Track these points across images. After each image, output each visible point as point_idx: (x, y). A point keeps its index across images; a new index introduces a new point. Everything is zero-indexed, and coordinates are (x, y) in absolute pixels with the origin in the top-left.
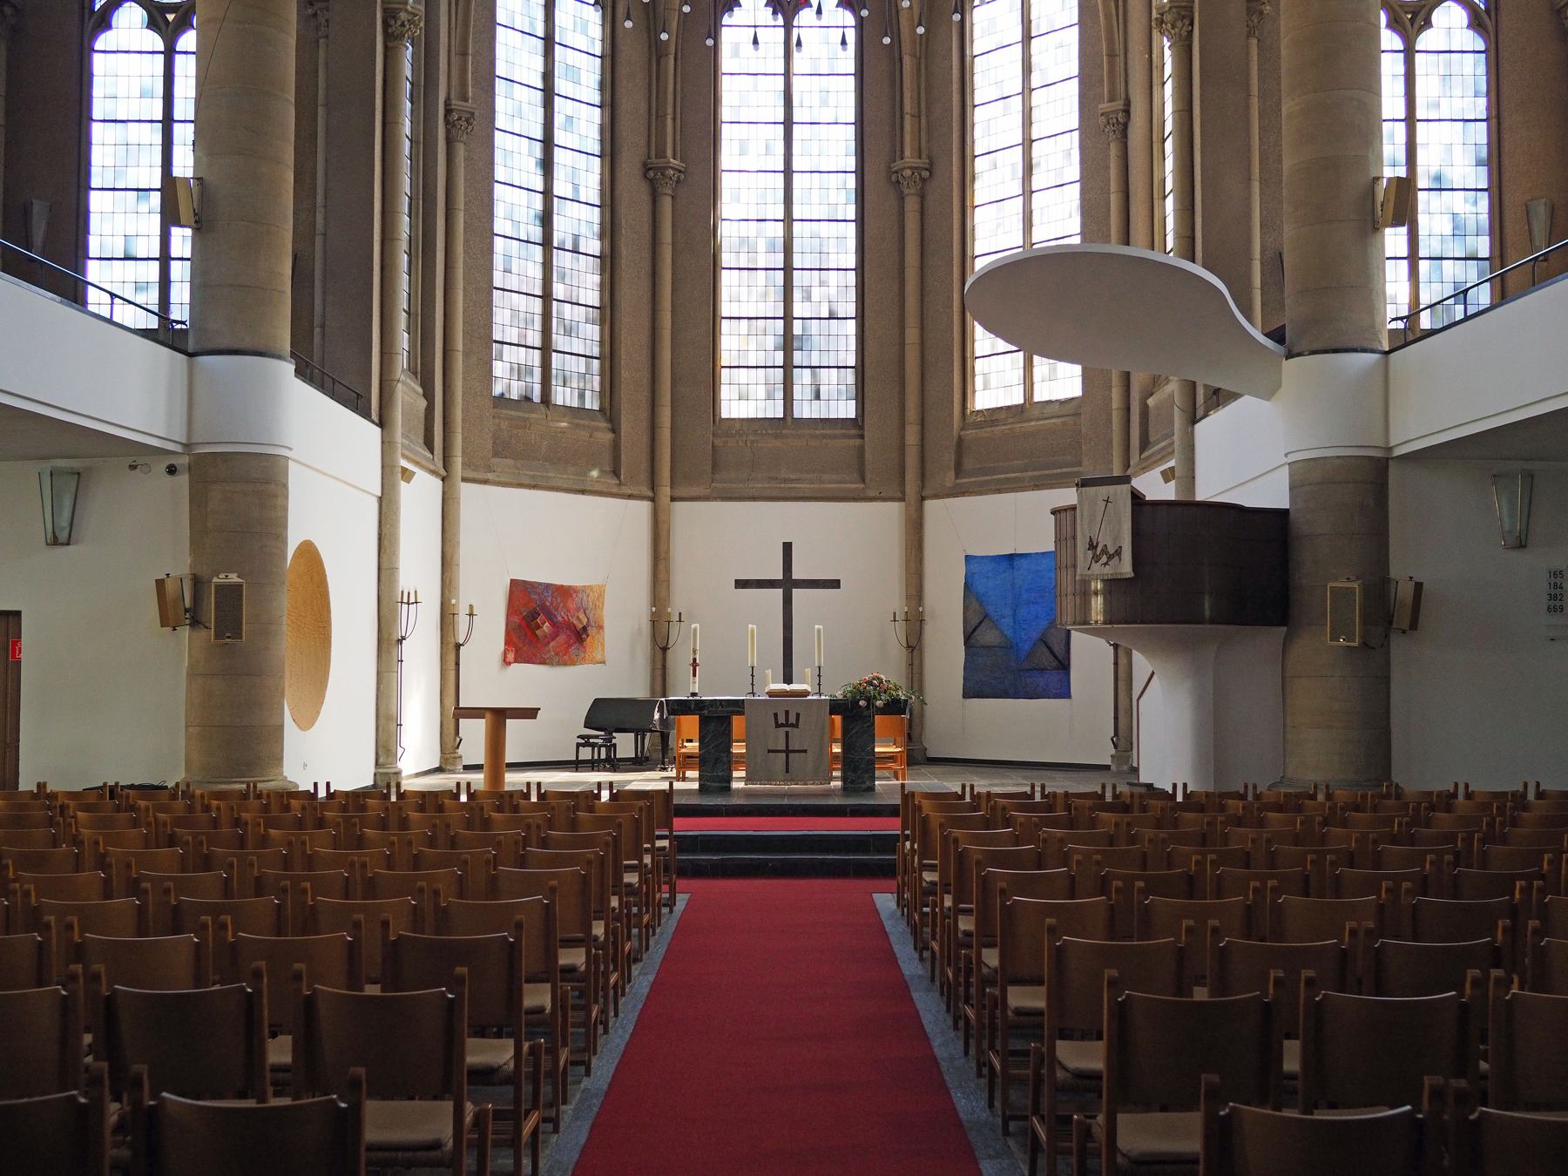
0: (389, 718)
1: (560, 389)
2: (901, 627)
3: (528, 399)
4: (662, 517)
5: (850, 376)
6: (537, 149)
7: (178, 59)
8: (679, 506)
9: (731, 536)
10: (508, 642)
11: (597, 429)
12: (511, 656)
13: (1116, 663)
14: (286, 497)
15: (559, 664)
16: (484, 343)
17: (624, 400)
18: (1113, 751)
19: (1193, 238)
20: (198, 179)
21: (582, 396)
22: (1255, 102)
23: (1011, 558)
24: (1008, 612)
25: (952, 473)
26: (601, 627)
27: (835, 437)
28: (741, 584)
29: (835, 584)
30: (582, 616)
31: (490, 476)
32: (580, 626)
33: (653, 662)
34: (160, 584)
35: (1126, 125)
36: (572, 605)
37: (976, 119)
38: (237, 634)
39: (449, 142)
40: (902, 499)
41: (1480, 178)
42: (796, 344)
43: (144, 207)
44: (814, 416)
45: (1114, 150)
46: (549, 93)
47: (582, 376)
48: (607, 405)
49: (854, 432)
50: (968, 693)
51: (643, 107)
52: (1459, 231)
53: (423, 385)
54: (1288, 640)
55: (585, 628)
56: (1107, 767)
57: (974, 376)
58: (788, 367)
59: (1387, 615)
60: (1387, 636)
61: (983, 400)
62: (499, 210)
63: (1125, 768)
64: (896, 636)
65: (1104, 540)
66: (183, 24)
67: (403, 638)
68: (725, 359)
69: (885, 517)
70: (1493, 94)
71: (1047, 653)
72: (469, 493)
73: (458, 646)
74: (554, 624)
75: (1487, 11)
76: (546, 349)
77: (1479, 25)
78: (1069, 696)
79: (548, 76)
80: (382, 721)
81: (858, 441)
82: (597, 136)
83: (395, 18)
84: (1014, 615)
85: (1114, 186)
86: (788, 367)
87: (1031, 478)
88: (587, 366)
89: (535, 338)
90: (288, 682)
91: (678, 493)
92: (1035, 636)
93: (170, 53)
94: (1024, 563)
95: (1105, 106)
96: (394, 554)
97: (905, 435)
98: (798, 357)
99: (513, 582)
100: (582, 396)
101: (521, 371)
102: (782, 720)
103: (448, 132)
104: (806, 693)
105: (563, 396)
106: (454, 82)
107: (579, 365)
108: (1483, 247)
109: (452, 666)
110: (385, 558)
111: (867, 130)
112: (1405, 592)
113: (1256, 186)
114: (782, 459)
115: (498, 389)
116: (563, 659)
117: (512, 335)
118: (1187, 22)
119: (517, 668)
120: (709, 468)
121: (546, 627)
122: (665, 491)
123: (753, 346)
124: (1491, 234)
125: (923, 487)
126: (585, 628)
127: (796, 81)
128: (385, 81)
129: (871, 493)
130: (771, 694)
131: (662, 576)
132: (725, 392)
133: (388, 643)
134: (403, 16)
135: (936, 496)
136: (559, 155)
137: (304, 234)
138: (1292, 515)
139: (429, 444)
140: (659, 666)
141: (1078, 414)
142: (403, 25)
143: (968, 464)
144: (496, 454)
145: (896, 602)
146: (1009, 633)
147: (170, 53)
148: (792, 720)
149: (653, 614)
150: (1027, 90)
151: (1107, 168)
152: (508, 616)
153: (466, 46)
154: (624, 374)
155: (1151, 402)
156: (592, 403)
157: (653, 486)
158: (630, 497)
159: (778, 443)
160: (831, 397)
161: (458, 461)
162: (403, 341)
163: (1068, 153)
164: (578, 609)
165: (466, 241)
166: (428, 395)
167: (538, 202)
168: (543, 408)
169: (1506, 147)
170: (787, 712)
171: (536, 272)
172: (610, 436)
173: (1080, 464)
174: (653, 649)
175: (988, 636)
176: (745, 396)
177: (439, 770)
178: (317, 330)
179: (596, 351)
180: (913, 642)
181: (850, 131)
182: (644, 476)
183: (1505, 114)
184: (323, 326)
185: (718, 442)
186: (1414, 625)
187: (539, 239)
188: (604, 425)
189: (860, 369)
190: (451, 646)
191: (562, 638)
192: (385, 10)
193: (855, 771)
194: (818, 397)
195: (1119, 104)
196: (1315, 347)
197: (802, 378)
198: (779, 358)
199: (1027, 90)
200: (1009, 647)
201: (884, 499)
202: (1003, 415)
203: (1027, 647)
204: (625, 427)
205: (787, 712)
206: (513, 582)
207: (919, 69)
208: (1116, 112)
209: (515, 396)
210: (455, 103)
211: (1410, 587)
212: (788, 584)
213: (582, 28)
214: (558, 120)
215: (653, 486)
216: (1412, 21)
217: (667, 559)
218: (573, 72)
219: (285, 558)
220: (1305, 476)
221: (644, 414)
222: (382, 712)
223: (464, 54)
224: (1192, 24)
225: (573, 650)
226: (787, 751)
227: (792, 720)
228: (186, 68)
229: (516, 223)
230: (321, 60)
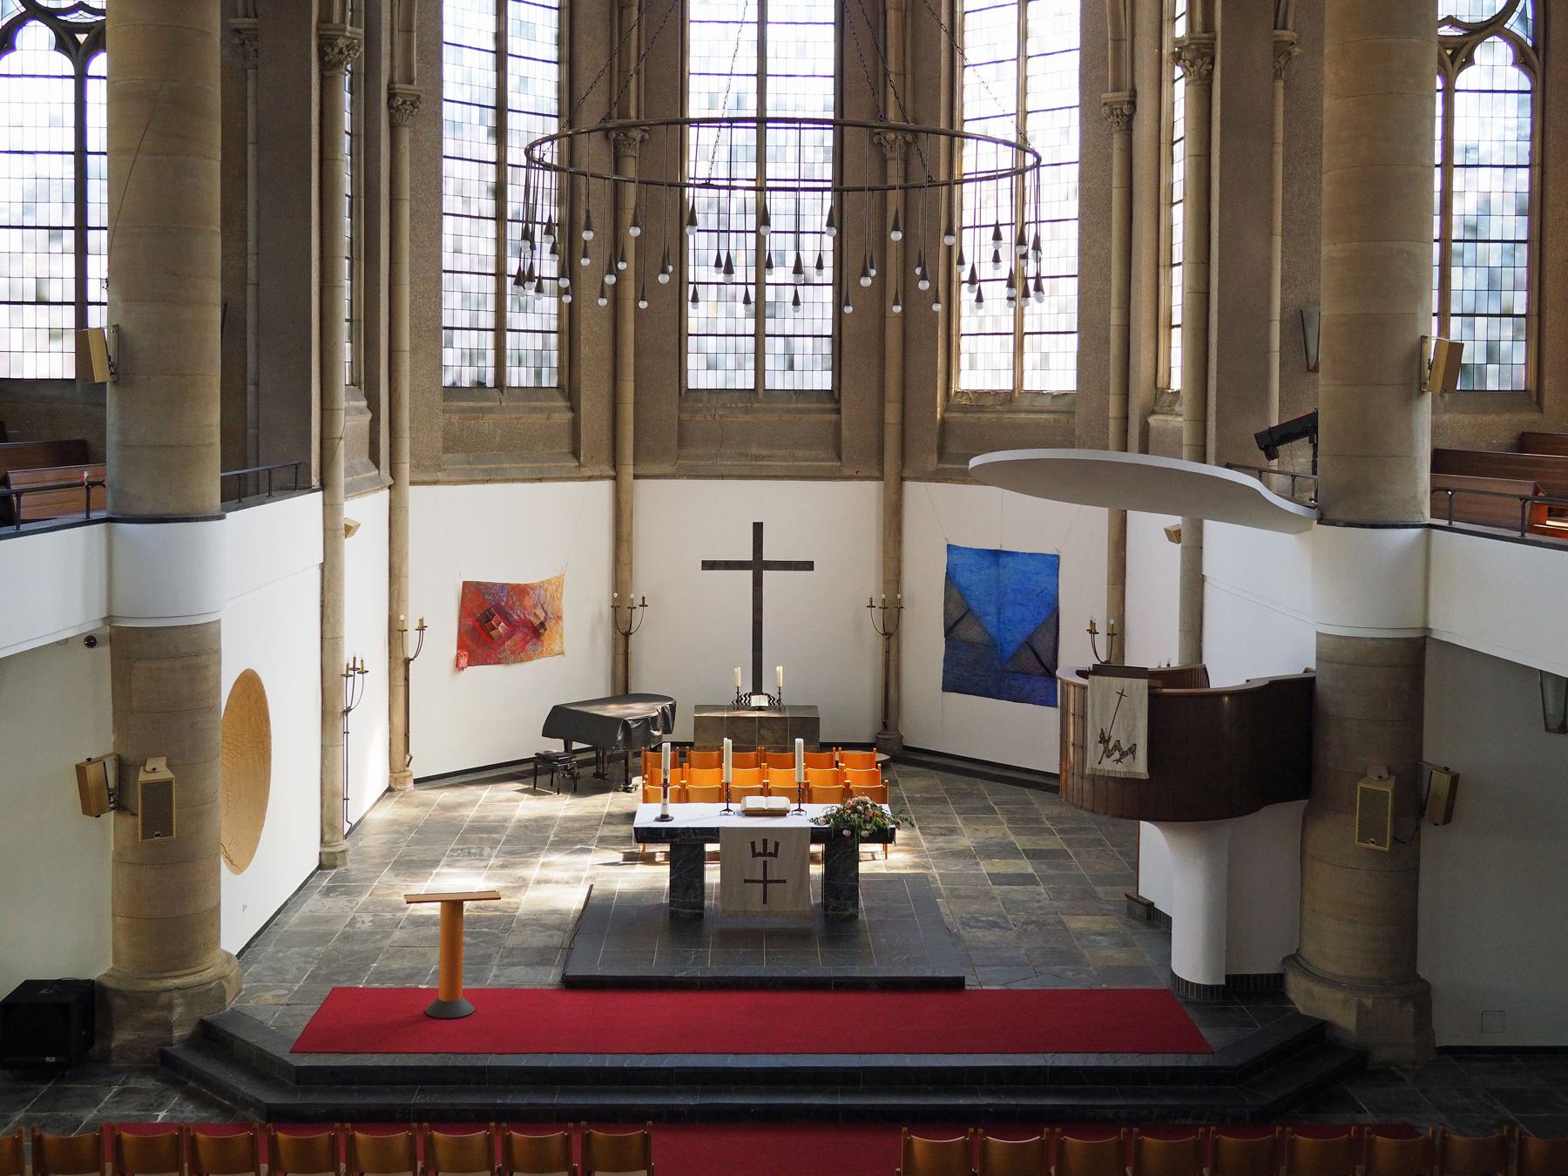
0: (334, 794)
2: (877, 614)
3: (480, 385)
4: (624, 497)
5: (826, 346)
6: (490, 116)
7: (90, 83)
8: (644, 485)
9: (696, 516)
11: (552, 410)
12: (464, 661)
14: (219, 663)
15: (515, 662)
16: (433, 332)
17: (583, 378)
19: (1208, 293)
20: (117, 329)
21: (538, 375)
22: (1279, 149)
23: (997, 554)
24: (992, 609)
26: (560, 618)
27: (809, 411)
28: (708, 565)
29: (808, 566)
32: (537, 622)
34: (81, 770)
35: (1130, 118)
36: (528, 602)
37: (966, 81)
38: (167, 831)
39: (394, 128)
41: (1518, 228)
42: (768, 312)
43: (56, 247)
44: (787, 387)
45: (1117, 142)
46: (501, 55)
47: (539, 354)
48: (566, 382)
49: (828, 406)
50: (948, 686)
51: (603, 62)
52: (1493, 286)
53: (367, 397)
54: (1307, 817)
55: (542, 624)
57: (959, 354)
58: (759, 336)
59: (1420, 803)
60: (1418, 828)
62: (449, 188)
65: (1118, 735)
66: (97, 41)
67: (348, 710)
70: (1537, 140)
72: (420, 499)
73: (407, 662)
74: (508, 623)
75: (1535, 47)
76: (500, 329)
77: (1525, 63)
79: (500, 37)
80: (327, 798)
81: (834, 417)
82: (554, 95)
83: (332, 46)
85: (1116, 181)
86: (759, 336)
88: (544, 343)
89: (488, 320)
90: (221, 799)
92: (1020, 638)
93: (81, 78)
95: (1109, 96)
96: (338, 623)
97: (887, 406)
98: (770, 326)
99: (465, 583)
100: (538, 375)
101: (472, 356)
102: (759, 849)
103: (392, 117)
105: (517, 376)
106: (397, 62)
107: (537, 341)
108: (1520, 302)
110: (327, 626)
111: (847, 85)
112: (1441, 783)
113: (1278, 241)
115: (448, 380)
116: (519, 656)
117: (463, 319)
118: (1207, 60)
120: (674, 443)
121: (502, 628)
122: (628, 470)
123: (722, 313)
124: (1528, 290)
125: (903, 466)
126: (542, 624)
127: (771, 30)
128: (321, 113)
129: (847, 472)
131: (624, 558)
132: (692, 361)
133: (333, 714)
134: (341, 42)
135: (918, 479)
136: (513, 121)
137: (234, 280)
138: (1319, 682)
139: (374, 457)
140: (621, 650)
141: (1071, 413)
142: (341, 52)
144: (446, 450)
145: (870, 584)
146: (992, 631)
147: (81, 78)
148: (771, 849)
149: (614, 600)
150: (1022, 57)
151: (1109, 157)
153: (411, 25)
154: (585, 350)
155: (1152, 420)
156: (549, 380)
157: (615, 463)
158: (590, 478)
159: (748, 418)
162: (345, 351)
163: (1067, 132)
164: (535, 606)
165: (413, 229)
166: (373, 406)
167: (490, 173)
169: (1551, 198)
170: (765, 841)
171: (489, 249)
172: (569, 415)
175: (972, 633)
176: (715, 365)
178: (251, 388)
179: (554, 326)
181: (829, 85)
182: (605, 454)
183: (1550, 163)
184: (257, 384)
185: (685, 417)
186: (1448, 819)
187: (491, 213)
188: (561, 403)
189: (837, 339)
190: (401, 661)
191: (519, 636)
192: (320, 37)
193: (837, 898)
194: (791, 368)
195: (1124, 95)
196: (1352, 517)
197: (775, 347)
198: (750, 326)
199: (1022, 57)
201: (861, 479)
202: (989, 401)
203: (1012, 648)
204: (585, 406)
205: (765, 841)
206: (465, 583)
207: (904, 25)
208: (1121, 103)
209: (466, 383)
210: (400, 87)
211: (1447, 778)
212: (758, 565)
213: (537, 30)
214: (512, 82)
215: (615, 463)
216: (1453, 58)
217: (630, 541)
218: (527, 27)
219: (214, 708)
220: (1330, 648)
221: (605, 388)
222: (326, 787)
223: (409, 31)
224: (1212, 62)
225: (529, 647)
226: (765, 882)
227: (771, 849)
228: (97, 93)
229: (467, 200)
230: (250, 93)
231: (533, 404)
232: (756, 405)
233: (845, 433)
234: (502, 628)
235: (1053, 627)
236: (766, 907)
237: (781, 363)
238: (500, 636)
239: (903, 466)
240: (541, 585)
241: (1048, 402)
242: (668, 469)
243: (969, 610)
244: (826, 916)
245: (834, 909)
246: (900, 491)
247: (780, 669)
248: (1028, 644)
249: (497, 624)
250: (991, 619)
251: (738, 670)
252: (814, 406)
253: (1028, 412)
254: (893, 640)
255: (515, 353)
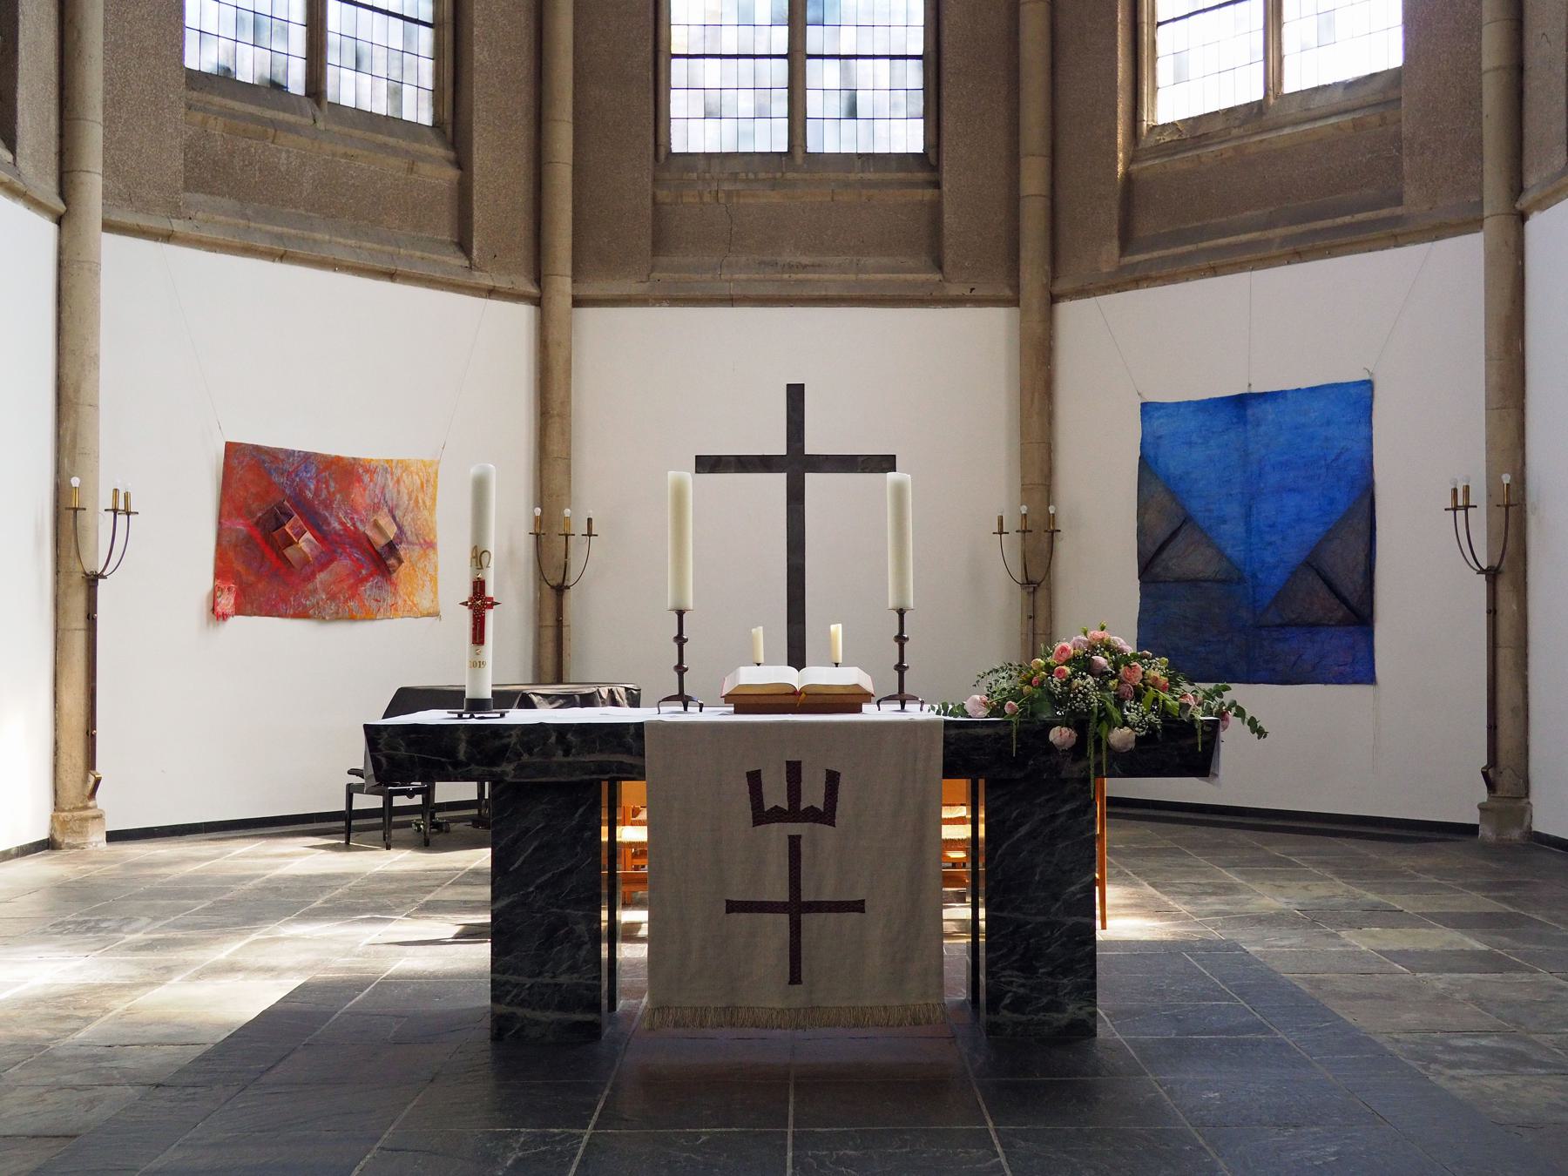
1: (348, 75)
2: (1013, 541)
3: (276, 87)
4: (555, 334)
5: (913, 75)
8: (589, 315)
9: (689, 372)
10: (220, 573)
11: (427, 158)
12: (227, 602)
13: (1493, 612)
15: (337, 617)
18: (1482, 794)
21: (395, 93)
23: (1241, 402)
24: (1233, 509)
25: (1114, 246)
26: (430, 545)
30: (384, 520)
31: (178, 226)
32: (380, 542)
33: (539, 614)
36: (361, 497)
40: (1014, 302)
48: (447, 116)
49: (921, 176)
55: (391, 547)
56: (1471, 830)
57: (1154, 59)
58: (796, 56)
61: (1173, 102)
63: (1515, 834)
64: (1000, 568)
68: (679, 41)
69: (978, 337)
71: (1323, 591)
72: (127, 267)
73: (92, 580)
74: (322, 536)
78: (1369, 677)
81: (928, 194)
84: (1248, 515)
86: (796, 56)
87: (1286, 240)
91: (589, 290)
92: (1293, 554)
94: (1269, 411)
98: (815, 39)
100: (395, 93)
102: (776, 796)
104: (851, 700)
109: (78, 622)
114: (786, 228)
116: (346, 606)
119: (238, 623)
120: (646, 243)
121: (306, 543)
122: (562, 286)
125: (1054, 276)
126: (391, 547)
130: (744, 701)
131: (555, 447)
132: (680, 104)
140: (549, 620)
143: (1146, 226)
145: (995, 490)
146: (1235, 552)
148: (813, 796)
149: (539, 521)
152: (222, 517)
154: (480, 54)
156: (418, 109)
157: (539, 276)
158: (492, 293)
159: (774, 197)
160: (879, 113)
161: (93, 186)
164: (376, 508)
168: (308, 105)
170: (794, 770)
172: (452, 173)
173: (1399, 200)
174: (539, 588)
175: (1191, 560)
176: (716, 110)
177: (49, 845)
180: (1036, 575)
182: (521, 255)
185: (664, 195)
188: (439, 151)
189: (934, 61)
190: (77, 577)
191: (342, 565)
193: (1027, 968)
194: (852, 113)
197: (823, 76)
198: (780, 40)
200: (1233, 579)
204: (481, 157)
205: (794, 770)
209: (245, 74)
212: (796, 463)
215: (539, 276)
217: (565, 416)
221: (521, 135)
225: (367, 589)
226: (796, 907)
227: (813, 796)
231: (381, 138)
232: (789, 175)
233: (949, 218)
234: (306, 543)
235: (1363, 526)
236: (798, 997)
237: (835, 105)
238: (305, 561)
239: (1054, 276)
240: (388, 467)
241: (1338, 95)
242: (632, 287)
243: (1187, 519)
244: (993, 1029)
245: (1018, 1005)
246: (1049, 320)
247: (837, 629)
248: (1312, 564)
249: (294, 534)
250: (1232, 531)
251: (759, 632)
252: (889, 176)
253: (1295, 123)
254: (1041, 593)
255: (349, 45)
